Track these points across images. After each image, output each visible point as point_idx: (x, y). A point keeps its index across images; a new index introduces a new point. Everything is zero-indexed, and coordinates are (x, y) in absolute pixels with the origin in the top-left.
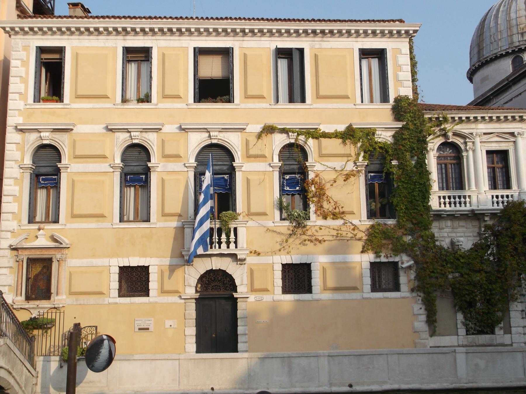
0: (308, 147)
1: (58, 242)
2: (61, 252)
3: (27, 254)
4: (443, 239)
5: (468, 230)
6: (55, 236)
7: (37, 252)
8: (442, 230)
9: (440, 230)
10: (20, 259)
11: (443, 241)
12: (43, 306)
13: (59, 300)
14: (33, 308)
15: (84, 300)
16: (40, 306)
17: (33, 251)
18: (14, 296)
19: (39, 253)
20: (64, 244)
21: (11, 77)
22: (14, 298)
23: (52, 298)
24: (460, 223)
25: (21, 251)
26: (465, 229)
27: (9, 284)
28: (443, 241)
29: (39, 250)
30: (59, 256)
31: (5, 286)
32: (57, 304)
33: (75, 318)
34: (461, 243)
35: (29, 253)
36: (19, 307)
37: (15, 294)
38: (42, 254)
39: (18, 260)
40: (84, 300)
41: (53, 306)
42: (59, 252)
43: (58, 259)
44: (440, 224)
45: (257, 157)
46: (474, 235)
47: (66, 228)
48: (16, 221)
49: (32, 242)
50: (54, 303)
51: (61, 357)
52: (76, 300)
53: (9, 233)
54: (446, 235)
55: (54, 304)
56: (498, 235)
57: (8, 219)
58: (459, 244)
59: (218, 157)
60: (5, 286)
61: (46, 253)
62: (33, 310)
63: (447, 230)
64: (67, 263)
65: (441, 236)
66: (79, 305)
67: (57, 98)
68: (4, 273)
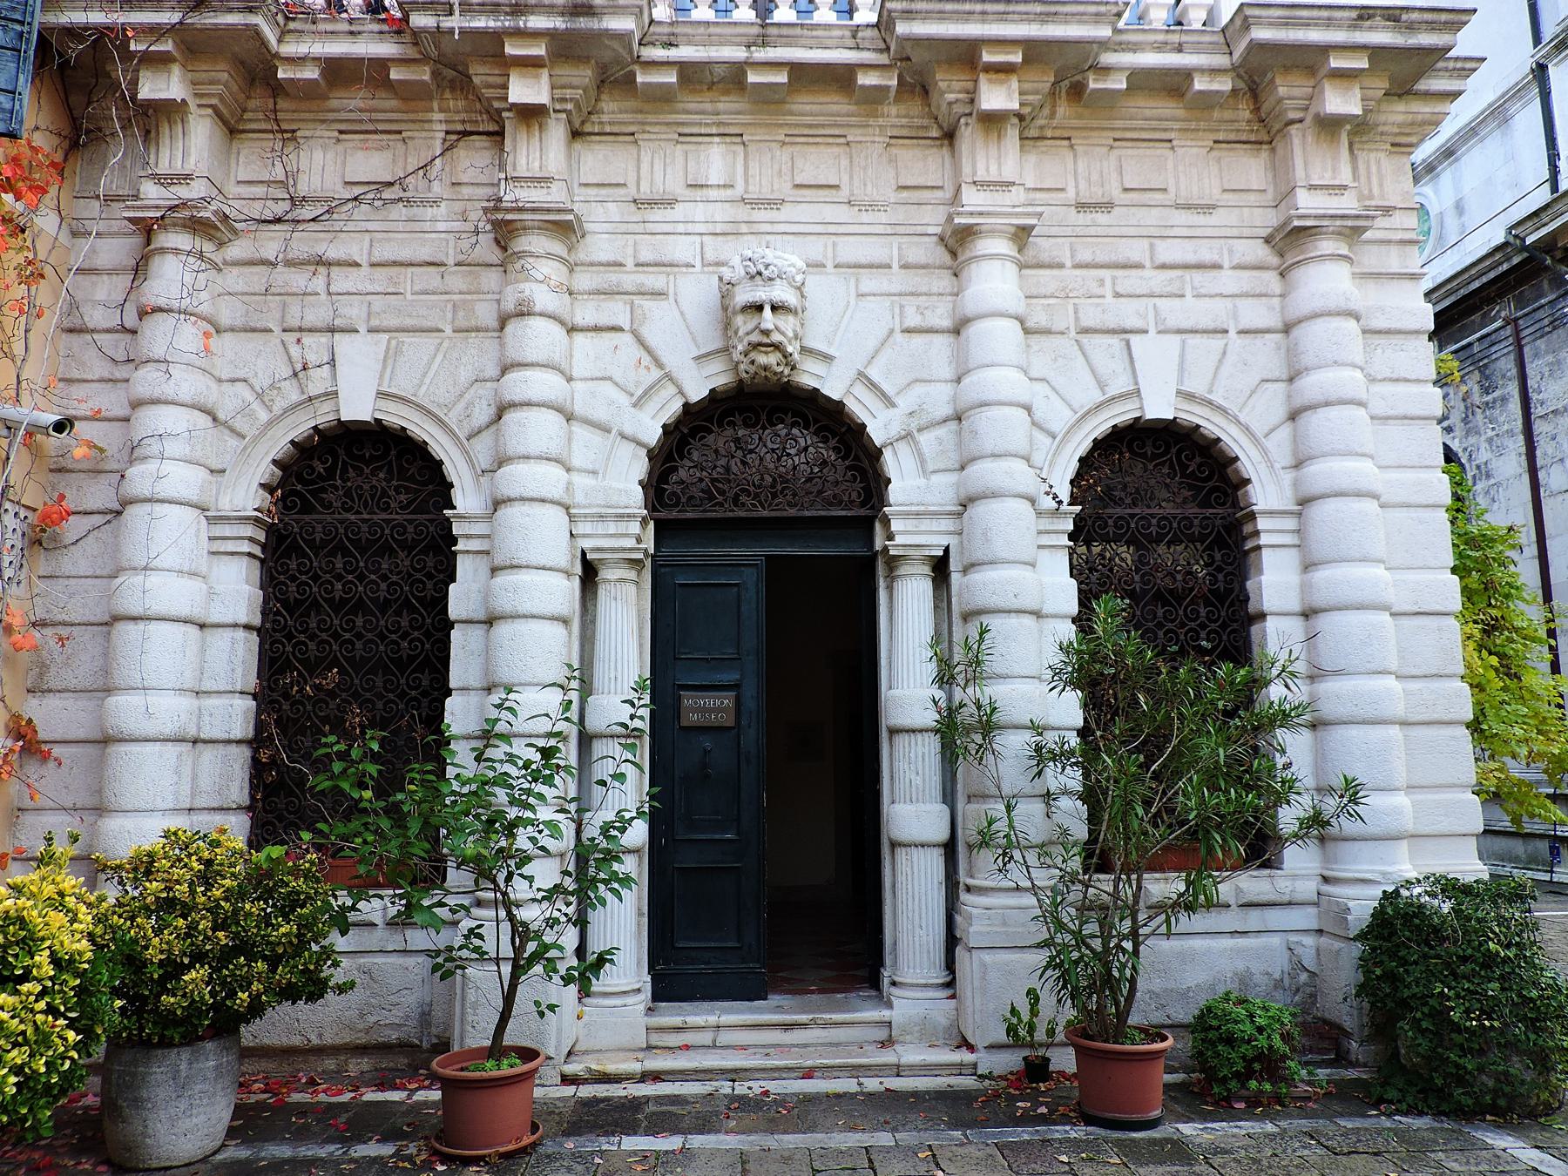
0: (168, 155)
4: (654, 280)
5: (865, 217)
8: (658, 214)
9: (638, 217)
11: (659, 294)
24: (799, 163)
26: (842, 213)
28: (659, 294)
34: (781, 293)
44: (645, 167)
46: (911, 260)
51: (256, 751)
54: (682, 250)
56: (1498, 895)
58: (761, 294)
59: (917, 908)
63: (696, 212)
65: (646, 256)
67: (874, 993)
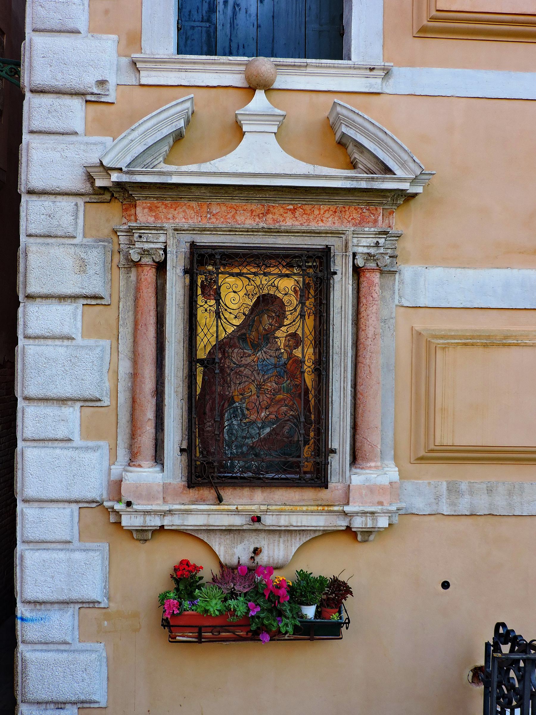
1: (353, 165)
2: (376, 221)
3: (181, 222)
6: (352, 124)
7: (240, 218)
10: (145, 252)
12: (283, 521)
13: (372, 489)
14: (229, 531)
15: (490, 491)
16: (269, 520)
17: (215, 209)
18: (113, 457)
19: (250, 223)
20: (399, 173)
21: (32, 132)
22: (117, 469)
23: (334, 482)
25: (151, 209)
27: (87, 394)
29: (249, 207)
30: (365, 242)
31: (63, 401)
32: (364, 513)
33: (446, 585)
35: (194, 221)
36: (155, 522)
37: (122, 454)
38: (269, 231)
39: (135, 257)
40: (490, 491)
41: (342, 523)
42: (362, 221)
43: (360, 262)
45: (247, 231)
47: (389, 87)
48: (115, 37)
49: (205, 161)
50: (347, 509)
52: (449, 490)
53: (77, 103)
55: (345, 514)
57: (71, 25)
60: (63, 401)
61: (289, 223)
62: (227, 539)
64: (402, 282)
66: (470, 520)
68: (57, 330)
